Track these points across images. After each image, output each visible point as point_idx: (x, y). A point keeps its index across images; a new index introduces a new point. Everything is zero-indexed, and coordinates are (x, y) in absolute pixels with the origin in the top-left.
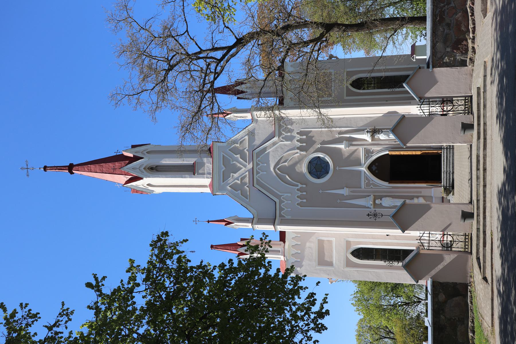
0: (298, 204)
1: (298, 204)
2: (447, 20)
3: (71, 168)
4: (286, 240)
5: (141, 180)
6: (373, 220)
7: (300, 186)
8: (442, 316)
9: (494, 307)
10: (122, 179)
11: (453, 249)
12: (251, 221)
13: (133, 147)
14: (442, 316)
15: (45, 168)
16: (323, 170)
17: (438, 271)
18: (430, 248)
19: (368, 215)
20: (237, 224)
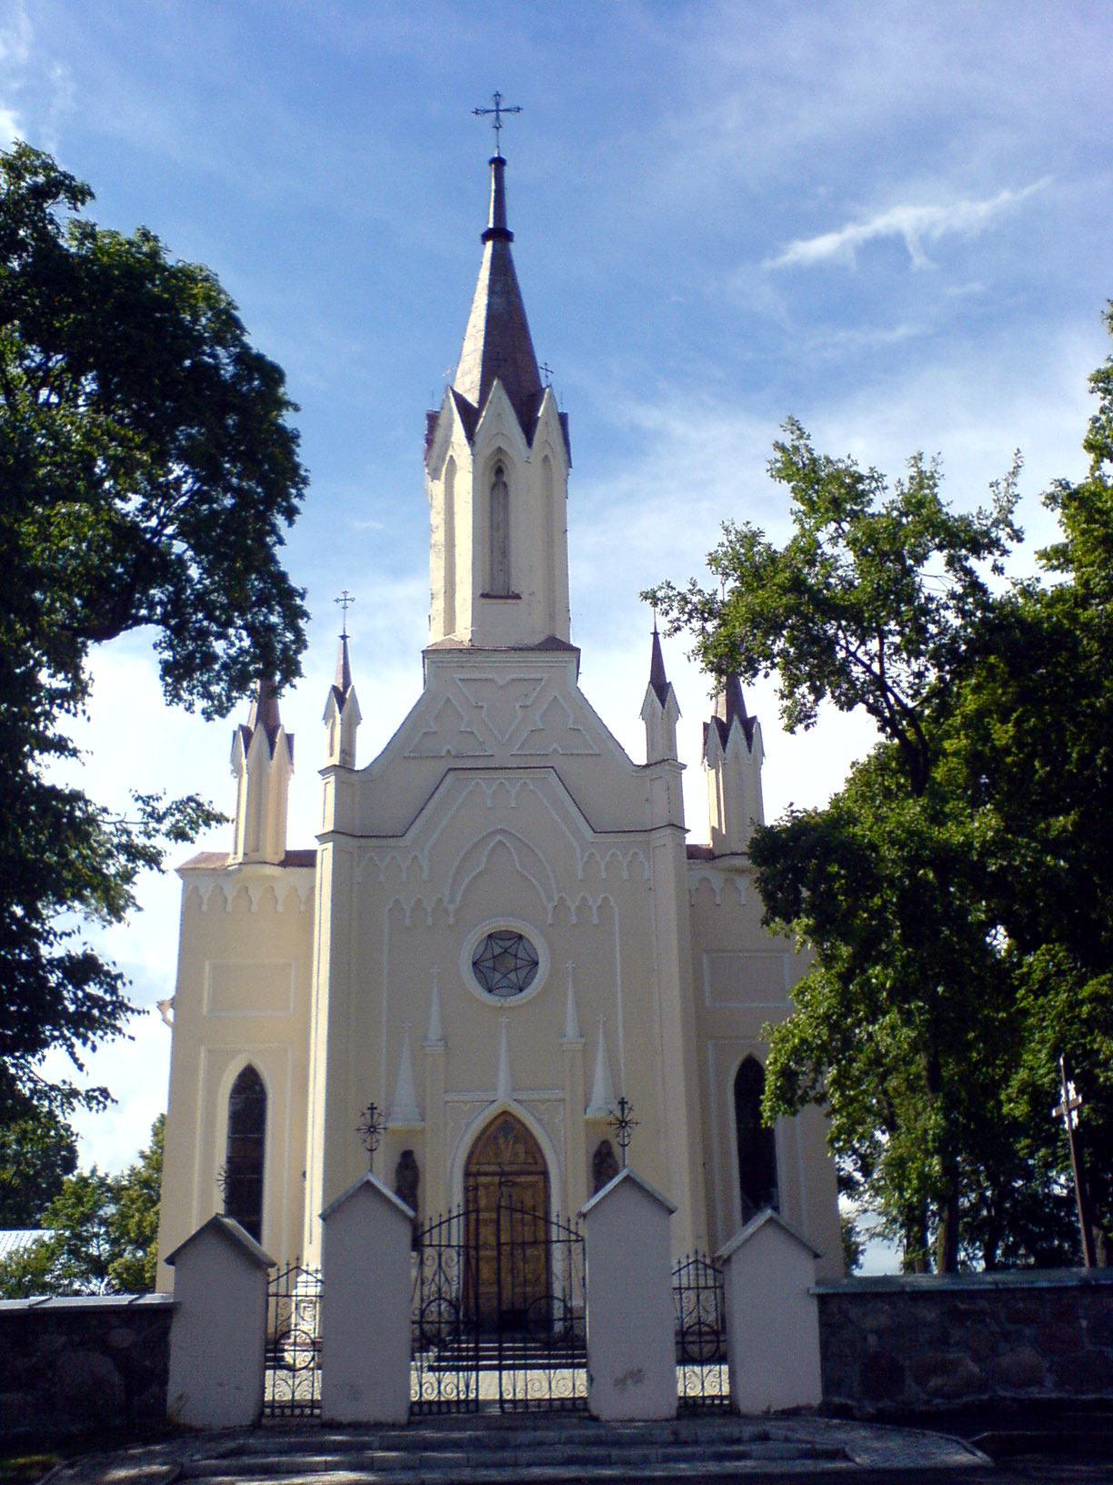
0: (397, 901)
1: (397, 901)
2: (956, 1334)
3: (499, 235)
4: (289, 870)
5: (464, 441)
6: (357, 1120)
7: (451, 908)
8: (63, 1339)
9: (456, 508)
10: (468, 380)
11: (269, 1373)
12: (343, 769)
13: (563, 419)
14: (63, 1339)
15: (499, 163)
16: (490, 963)
17: (470, 330)
18: (272, 1300)
19: (372, 1108)
20: (338, 721)
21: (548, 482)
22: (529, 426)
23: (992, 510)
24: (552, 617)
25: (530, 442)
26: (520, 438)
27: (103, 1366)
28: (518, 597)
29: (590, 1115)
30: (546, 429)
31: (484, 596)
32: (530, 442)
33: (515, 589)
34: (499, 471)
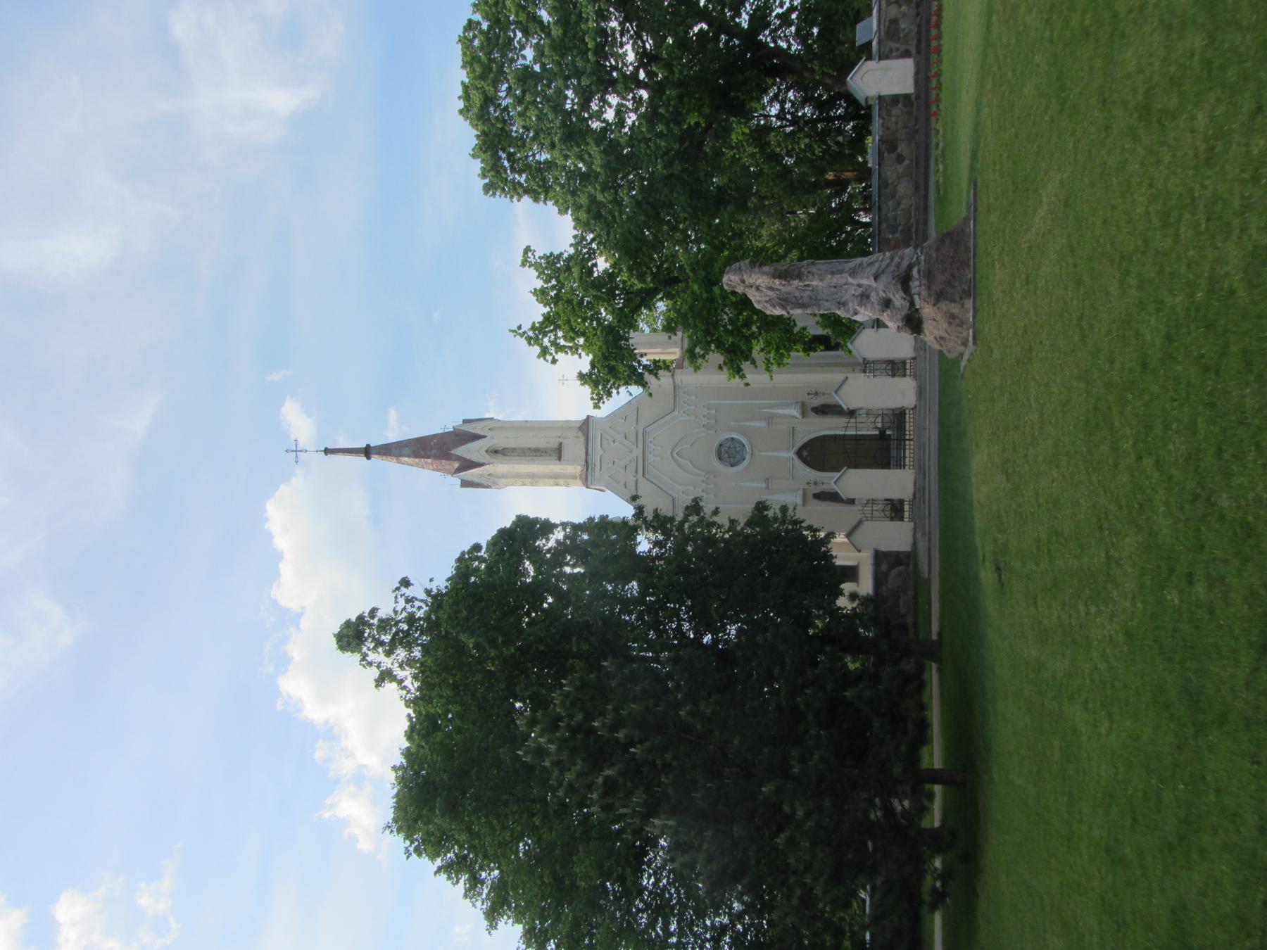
21: (500, 428)
22: (476, 437)
23: (374, 669)
24: (569, 428)
25: (484, 437)
26: (484, 440)
27: (893, 573)
28: (561, 444)
29: (798, 416)
30: (471, 428)
31: (560, 459)
32: (484, 437)
33: (556, 445)
34: (496, 452)
